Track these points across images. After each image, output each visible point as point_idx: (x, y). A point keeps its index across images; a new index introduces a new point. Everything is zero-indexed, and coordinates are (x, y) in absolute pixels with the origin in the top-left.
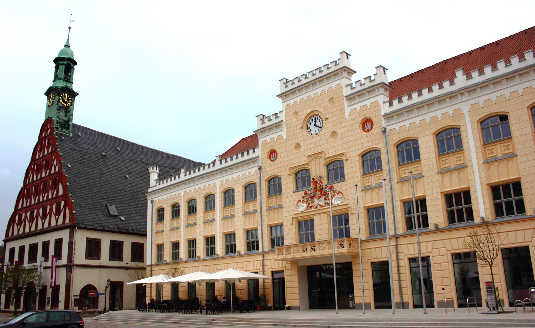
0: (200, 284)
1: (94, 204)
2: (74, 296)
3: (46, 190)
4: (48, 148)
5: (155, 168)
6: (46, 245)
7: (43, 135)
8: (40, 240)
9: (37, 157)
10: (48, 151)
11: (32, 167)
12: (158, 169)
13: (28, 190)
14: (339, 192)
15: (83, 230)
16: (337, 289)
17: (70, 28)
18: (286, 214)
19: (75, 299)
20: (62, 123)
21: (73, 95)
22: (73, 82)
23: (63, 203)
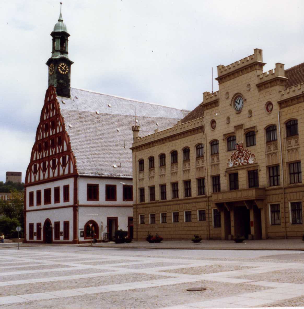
1: (92, 156)
2: (80, 229)
3: (53, 146)
4: (53, 110)
6: (57, 190)
7: (48, 100)
8: (52, 186)
9: (45, 118)
10: (53, 114)
11: (42, 126)
13: (40, 145)
14: (252, 154)
15: (97, 179)
17: (61, 3)
18: (221, 169)
19: (81, 232)
21: (69, 63)
22: (68, 52)
23: (67, 157)
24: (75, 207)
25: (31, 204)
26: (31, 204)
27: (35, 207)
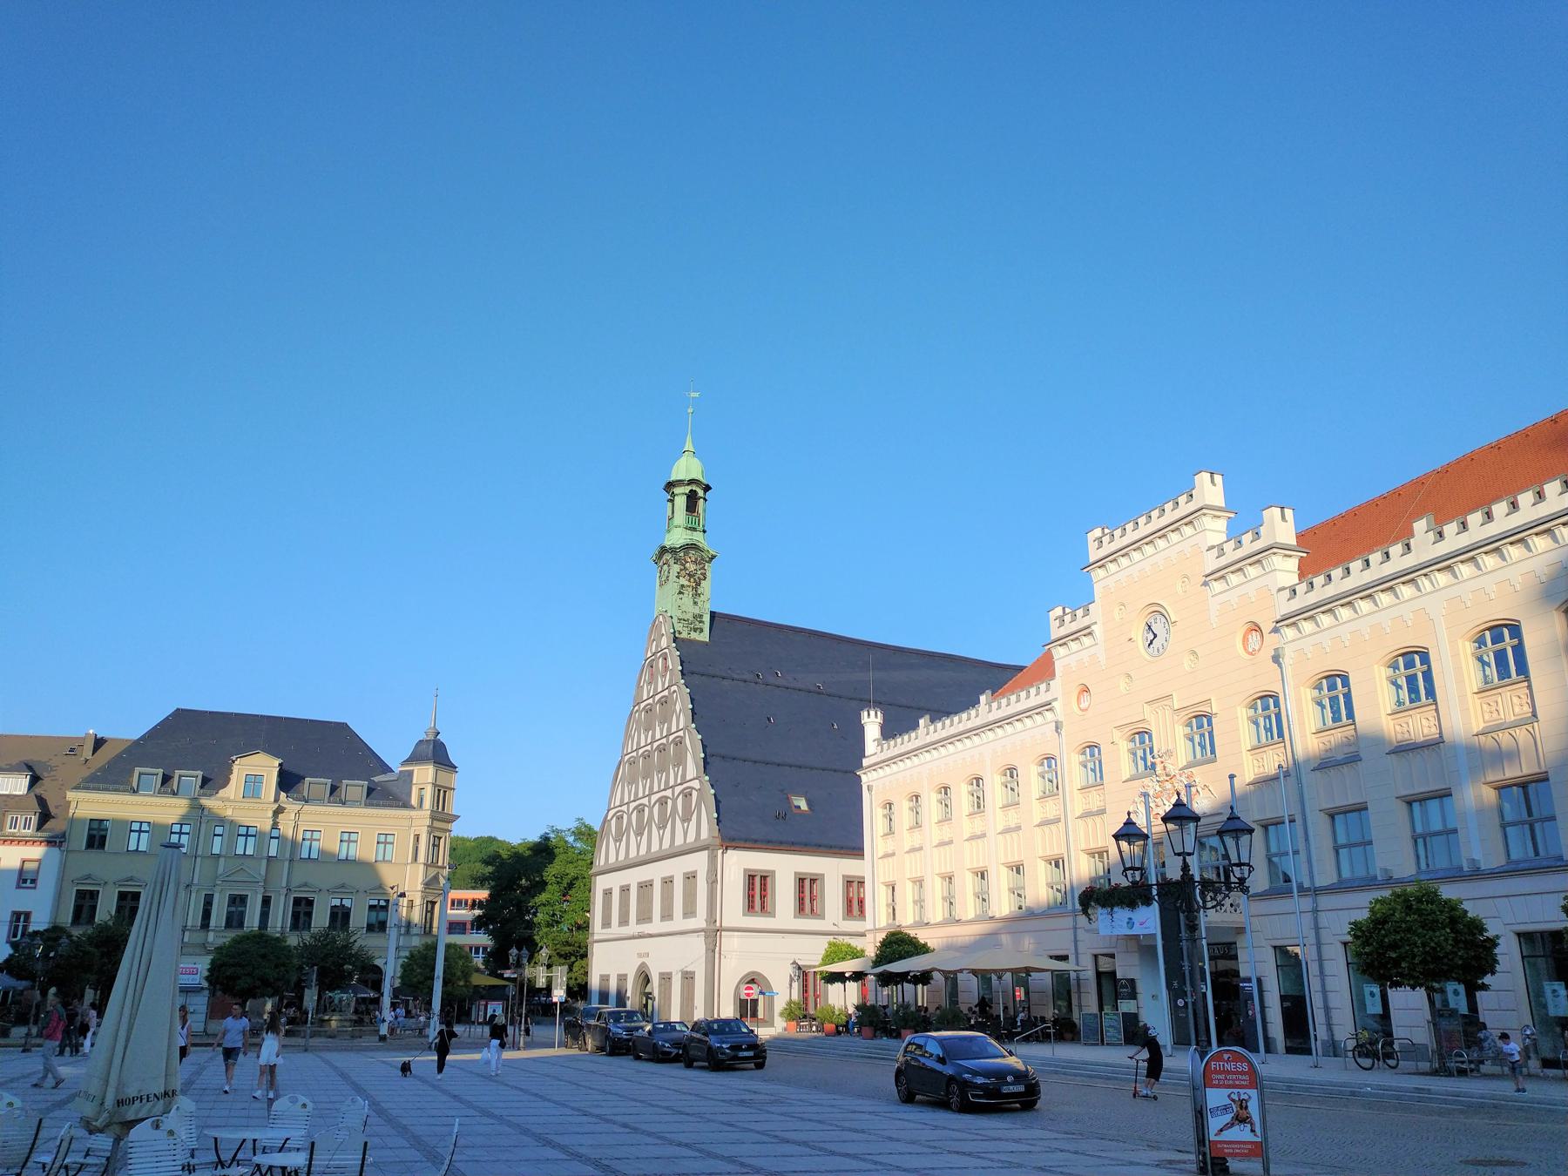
0: (1000, 978)
5: (872, 713)
8: (655, 872)
12: (879, 713)
16: (1216, 1002)
20: (688, 620)
24: (713, 934)
25: (606, 923)
26: (606, 923)
27: (616, 929)
